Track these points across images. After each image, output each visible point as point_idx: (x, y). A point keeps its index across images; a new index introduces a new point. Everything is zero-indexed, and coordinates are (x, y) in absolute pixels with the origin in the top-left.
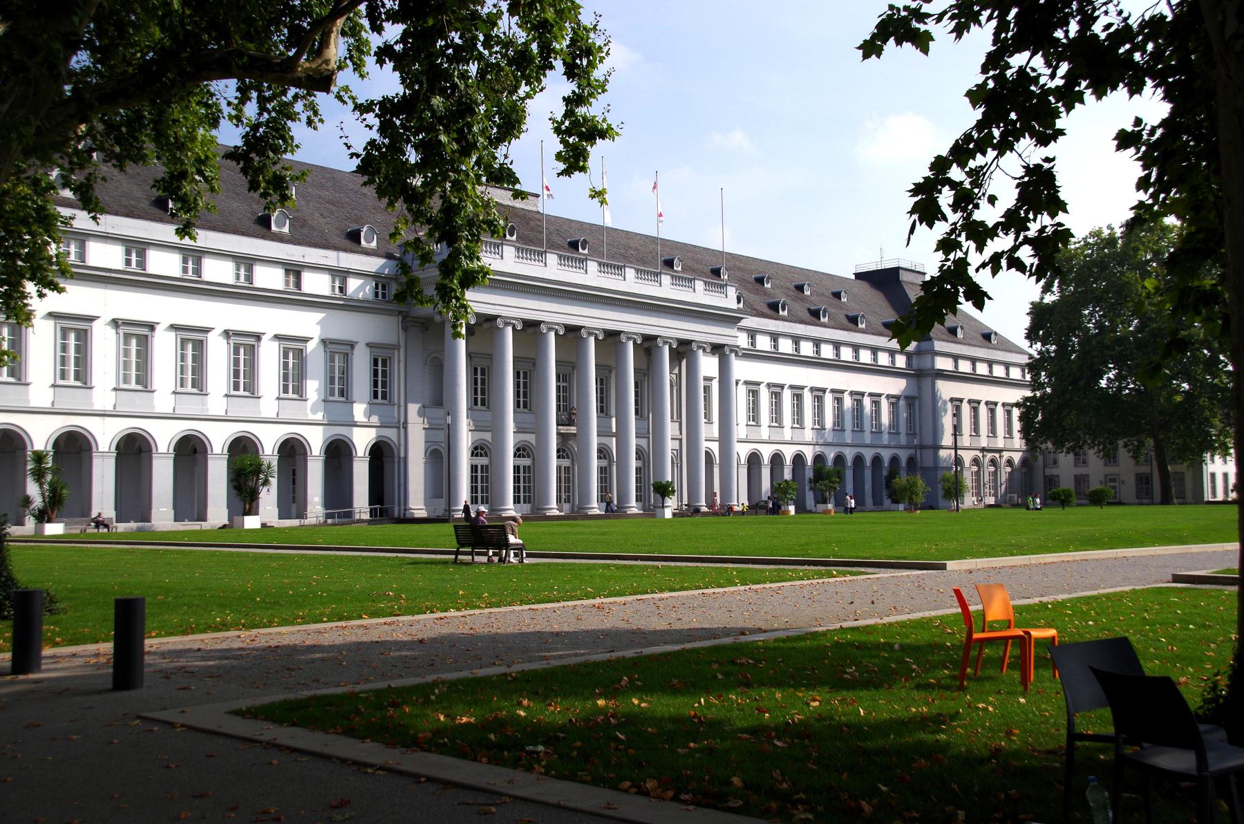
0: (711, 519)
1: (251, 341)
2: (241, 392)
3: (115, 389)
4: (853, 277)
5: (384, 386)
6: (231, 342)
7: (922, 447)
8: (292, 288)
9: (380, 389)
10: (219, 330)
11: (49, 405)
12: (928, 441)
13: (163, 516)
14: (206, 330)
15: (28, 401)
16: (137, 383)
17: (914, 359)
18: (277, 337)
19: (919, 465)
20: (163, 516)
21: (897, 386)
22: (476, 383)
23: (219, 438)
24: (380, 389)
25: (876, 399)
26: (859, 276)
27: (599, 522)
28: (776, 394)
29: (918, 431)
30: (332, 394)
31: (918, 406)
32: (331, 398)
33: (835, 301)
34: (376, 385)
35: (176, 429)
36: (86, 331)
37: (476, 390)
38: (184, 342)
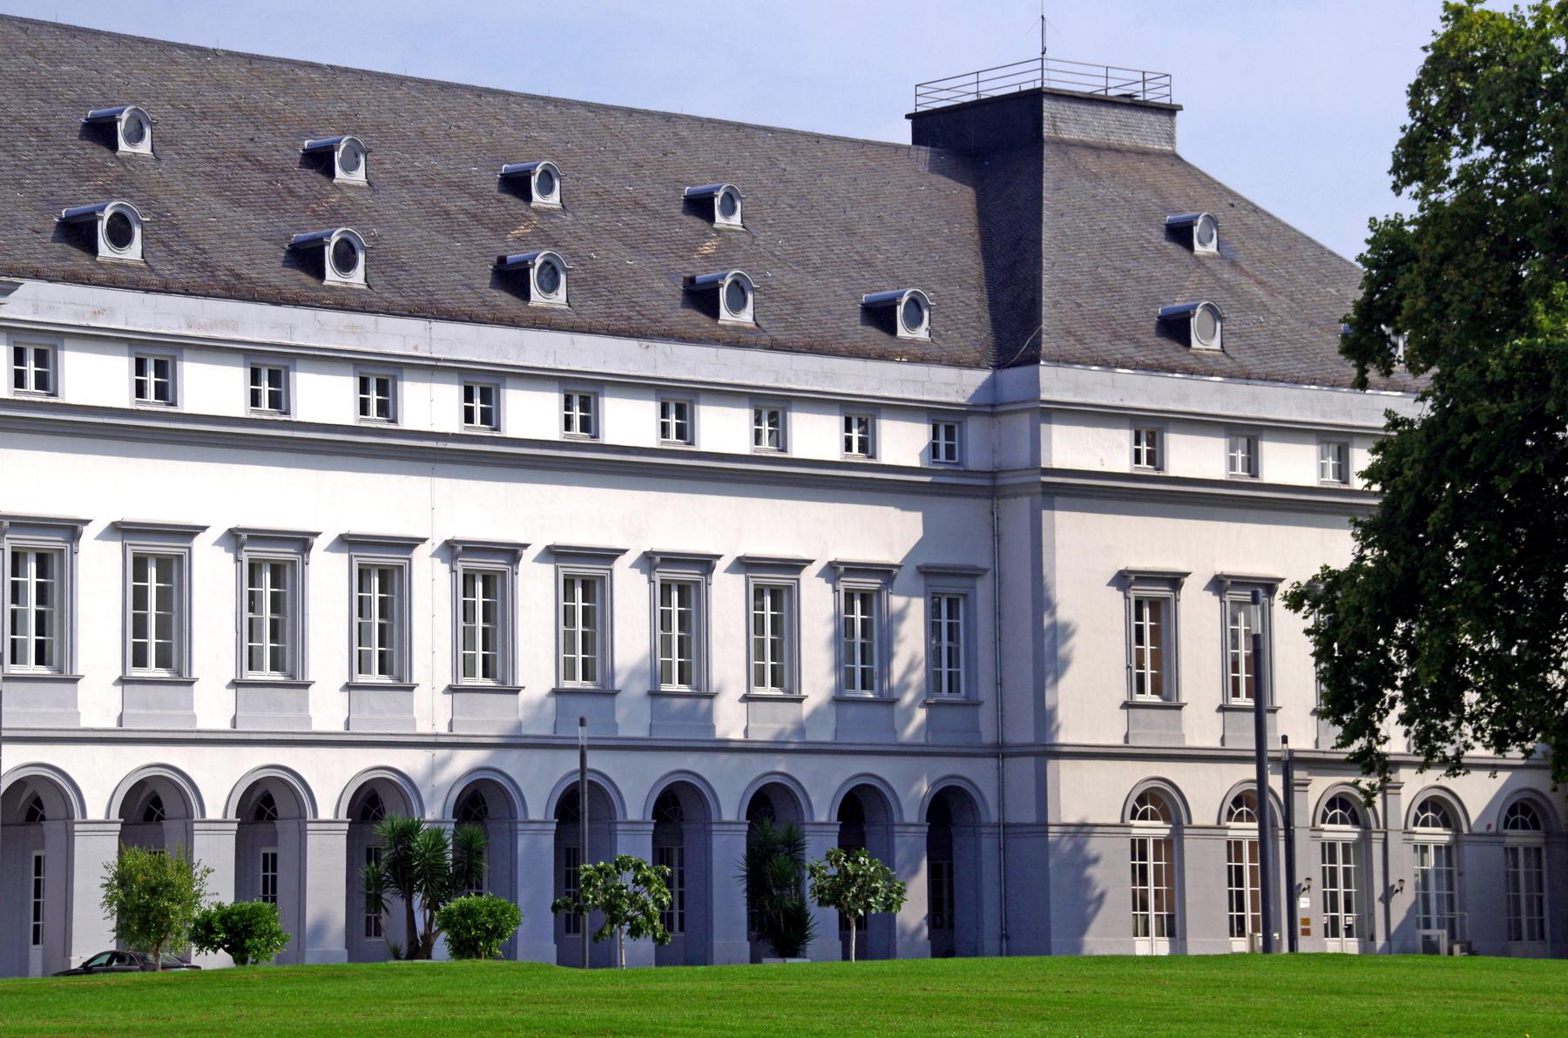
0: (86, 979)
1: (1161, 591)
2: (152, 671)
3: (451, 690)
4: (903, 134)
5: (163, 629)
6: (460, 567)
7: (1001, 751)
8: (1240, 474)
9: (152, 641)
10: (217, 531)
11: (113, 724)
12: (1022, 734)
13: (1210, 933)
14: (188, 533)
15: (309, 720)
16: (274, 667)
17: (973, 430)
18: (121, 530)
19: (990, 813)
20: (1210, 933)
21: (886, 534)
22: (759, 628)
23: (329, 780)
24: (152, 641)
25: (952, 586)
26: (927, 125)
27: (78, 978)
28: (1157, 605)
29: (985, 691)
30: (140, 661)
31: (982, 603)
32: (466, 682)
33: (98, 153)
34: (140, 627)
35: (127, 763)
36: (180, 557)
37: (570, 637)
38: (140, 564)
